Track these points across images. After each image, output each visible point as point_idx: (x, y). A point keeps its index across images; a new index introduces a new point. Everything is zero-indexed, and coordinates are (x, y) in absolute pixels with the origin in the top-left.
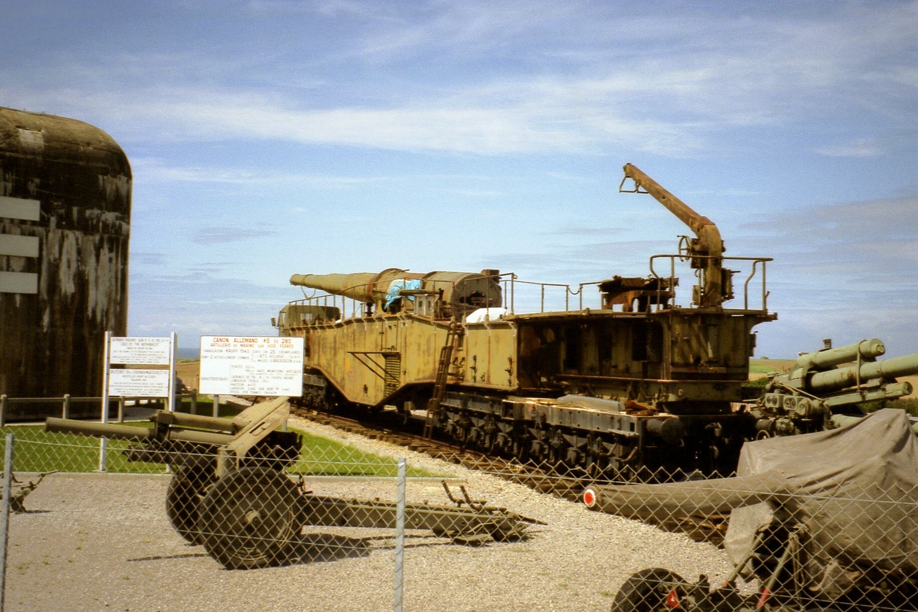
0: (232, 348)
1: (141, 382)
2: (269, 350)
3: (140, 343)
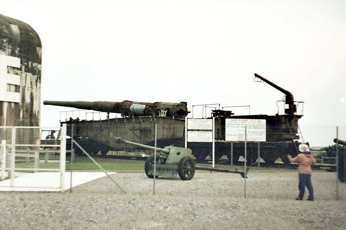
0: (238, 123)
1: (201, 136)
2: (253, 124)
3: (200, 121)
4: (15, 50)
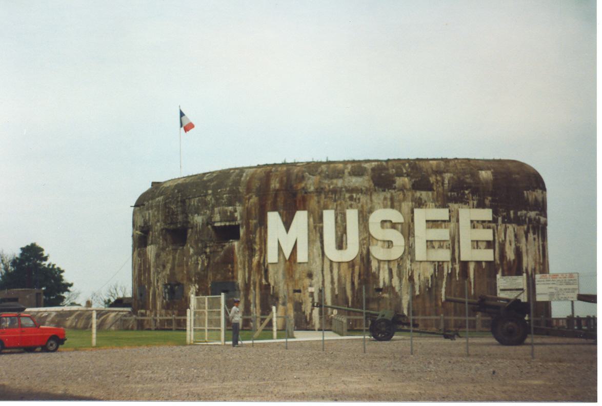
4: (484, 201)
